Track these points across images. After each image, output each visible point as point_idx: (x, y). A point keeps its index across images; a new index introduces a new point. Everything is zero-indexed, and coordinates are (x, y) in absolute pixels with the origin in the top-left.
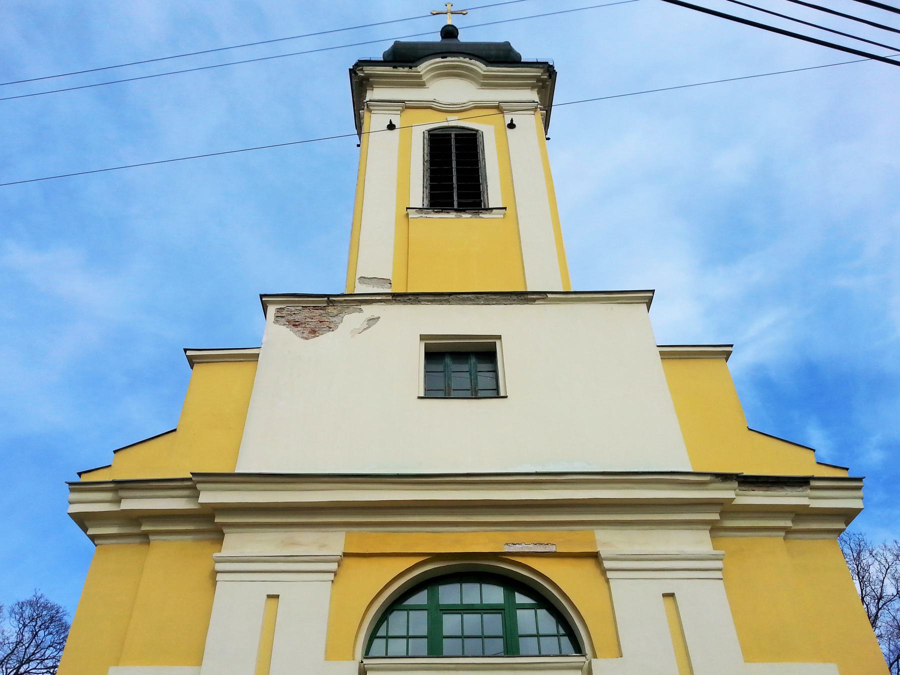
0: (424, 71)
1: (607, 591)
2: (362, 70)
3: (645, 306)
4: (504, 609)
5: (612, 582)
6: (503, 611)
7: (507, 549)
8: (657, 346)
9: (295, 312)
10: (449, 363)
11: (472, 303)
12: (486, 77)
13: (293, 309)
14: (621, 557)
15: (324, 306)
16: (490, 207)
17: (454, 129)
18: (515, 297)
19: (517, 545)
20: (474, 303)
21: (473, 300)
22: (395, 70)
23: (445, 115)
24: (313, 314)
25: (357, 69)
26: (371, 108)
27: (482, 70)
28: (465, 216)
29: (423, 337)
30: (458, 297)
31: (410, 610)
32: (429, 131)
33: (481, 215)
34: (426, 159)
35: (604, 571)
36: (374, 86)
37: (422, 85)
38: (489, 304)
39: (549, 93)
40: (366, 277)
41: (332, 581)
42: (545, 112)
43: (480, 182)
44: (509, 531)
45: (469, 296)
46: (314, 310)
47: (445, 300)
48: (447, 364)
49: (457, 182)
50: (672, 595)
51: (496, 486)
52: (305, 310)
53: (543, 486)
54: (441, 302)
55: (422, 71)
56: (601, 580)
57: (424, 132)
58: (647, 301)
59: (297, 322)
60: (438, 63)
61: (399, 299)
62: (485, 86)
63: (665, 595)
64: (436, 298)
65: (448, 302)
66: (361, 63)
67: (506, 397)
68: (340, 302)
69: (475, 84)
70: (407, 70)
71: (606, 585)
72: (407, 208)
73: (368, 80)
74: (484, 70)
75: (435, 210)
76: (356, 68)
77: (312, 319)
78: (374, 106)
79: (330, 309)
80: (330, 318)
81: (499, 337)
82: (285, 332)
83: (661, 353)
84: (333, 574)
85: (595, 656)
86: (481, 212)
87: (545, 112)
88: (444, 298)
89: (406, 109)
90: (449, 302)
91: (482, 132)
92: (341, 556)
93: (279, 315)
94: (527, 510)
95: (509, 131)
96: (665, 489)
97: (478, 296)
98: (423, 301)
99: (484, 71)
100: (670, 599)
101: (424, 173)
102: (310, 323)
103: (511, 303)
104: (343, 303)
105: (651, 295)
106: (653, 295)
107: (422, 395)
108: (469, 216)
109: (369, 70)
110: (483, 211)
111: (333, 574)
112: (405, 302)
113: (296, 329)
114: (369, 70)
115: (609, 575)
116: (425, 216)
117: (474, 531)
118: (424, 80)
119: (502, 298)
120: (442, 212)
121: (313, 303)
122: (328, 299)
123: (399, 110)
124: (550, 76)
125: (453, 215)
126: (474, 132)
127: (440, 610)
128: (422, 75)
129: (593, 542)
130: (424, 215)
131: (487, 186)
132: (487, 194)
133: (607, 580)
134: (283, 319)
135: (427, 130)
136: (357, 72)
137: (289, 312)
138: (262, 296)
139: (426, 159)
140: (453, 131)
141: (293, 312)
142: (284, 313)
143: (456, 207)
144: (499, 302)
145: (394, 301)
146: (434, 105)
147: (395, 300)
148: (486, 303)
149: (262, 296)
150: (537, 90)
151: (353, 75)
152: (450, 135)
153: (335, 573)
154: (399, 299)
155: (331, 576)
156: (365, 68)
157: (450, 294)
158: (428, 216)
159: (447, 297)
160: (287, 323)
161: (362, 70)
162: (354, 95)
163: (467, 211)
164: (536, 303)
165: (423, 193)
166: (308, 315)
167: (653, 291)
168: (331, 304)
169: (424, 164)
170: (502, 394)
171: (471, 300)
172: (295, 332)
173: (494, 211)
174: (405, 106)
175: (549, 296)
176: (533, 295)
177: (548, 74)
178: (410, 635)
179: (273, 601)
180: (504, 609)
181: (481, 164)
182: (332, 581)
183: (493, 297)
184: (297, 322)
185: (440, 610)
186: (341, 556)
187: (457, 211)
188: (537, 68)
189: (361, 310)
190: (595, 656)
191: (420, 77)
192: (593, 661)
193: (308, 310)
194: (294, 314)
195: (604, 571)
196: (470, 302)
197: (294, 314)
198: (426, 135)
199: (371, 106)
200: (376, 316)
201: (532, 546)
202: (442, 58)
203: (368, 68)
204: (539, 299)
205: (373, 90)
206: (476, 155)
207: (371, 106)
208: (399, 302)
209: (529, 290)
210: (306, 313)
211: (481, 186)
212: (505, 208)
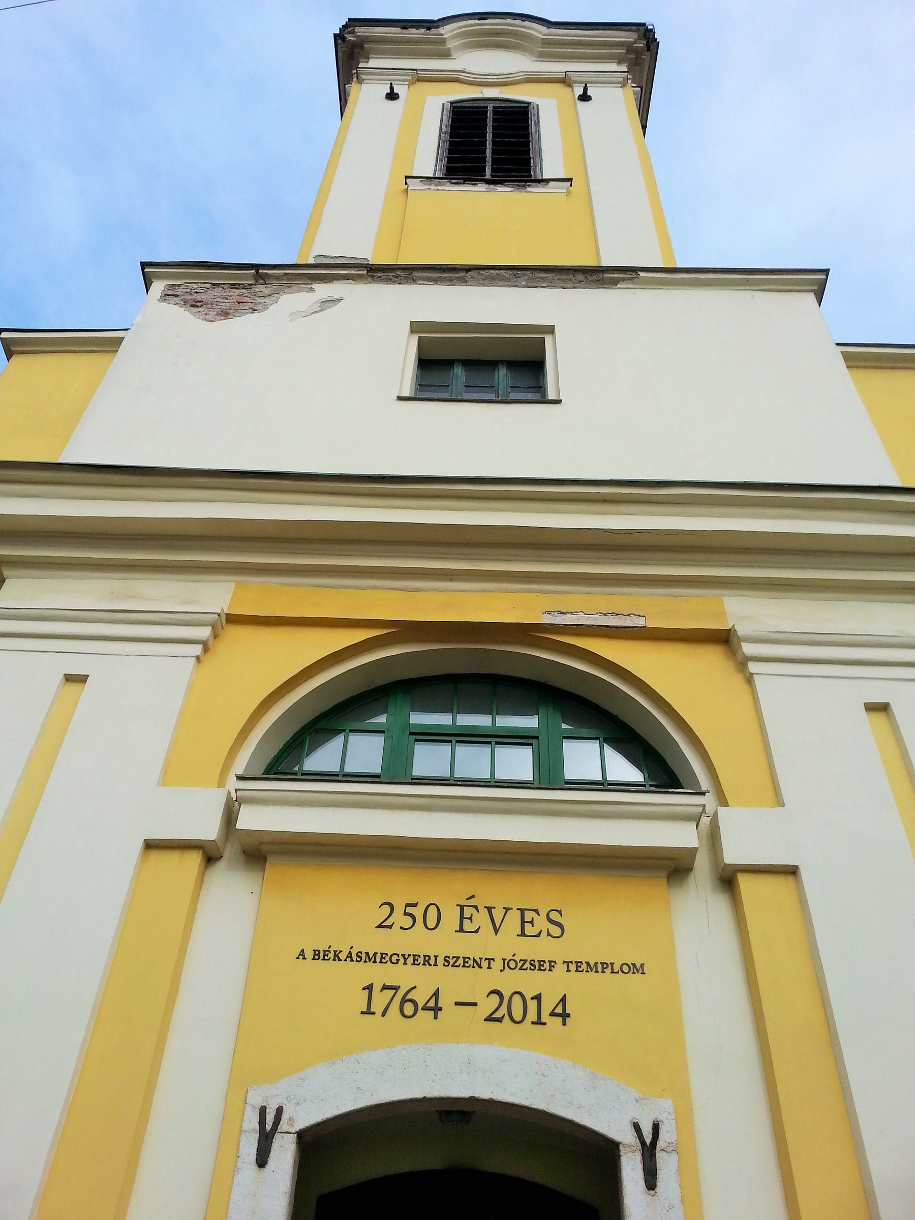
0: (450, 34)
1: (748, 701)
2: (353, 32)
3: (811, 297)
4: (537, 738)
5: (757, 680)
6: (535, 742)
7: (547, 620)
8: (837, 344)
9: (198, 291)
10: (460, 374)
11: (506, 283)
12: (546, 43)
13: (195, 286)
14: (779, 636)
15: (249, 285)
16: (544, 177)
17: (492, 102)
18: (581, 277)
19: (568, 615)
20: (509, 283)
21: (509, 280)
22: (404, 31)
23: (480, 88)
24: (228, 294)
25: (346, 30)
26: (363, 77)
27: (540, 33)
28: (500, 188)
29: (416, 327)
30: (483, 274)
31: (351, 731)
32: (452, 103)
33: (528, 189)
34: (444, 130)
35: (742, 663)
36: (370, 56)
37: (446, 55)
38: (536, 287)
39: (646, 73)
40: (328, 254)
41: (198, 658)
42: (639, 89)
43: (530, 155)
44: (554, 592)
45: (501, 271)
46: (231, 290)
47: (458, 279)
48: (458, 374)
49: (493, 154)
50: (883, 708)
51: (531, 505)
52: (215, 290)
53: (623, 508)
54: (451, 282)
55: (446, 33)
56: (738, 680)
57: (443, 104)
58: (816, 288)
59: (200, 302)
60: (472, 25)
61: (379, 275)
62: (544, 56)
63: (871, 708)
64: (444, 275)
65: (463, 281)
66: (353, 23)
67: (558, 402)
68: (277, 278)
69: (527, 54)
70: (424, 32)
71: (746, 688)
72: (406, 177)
73: (362, 48)
74: (544, 33)
75: (453, 181)
76: (344, 31)
77: (227, 299)
78: (367, 74)
79: (260, 288)
80: (258, 298)
81: (551, 330)
82: (177, 313)
83: (846, 356)
84: (201, 646)
85: (723, 801)
86: (529, 186)
87: (639, 89)
88: (457, 275)
89: (419, 83)
90: (466, 281)
91: (537, 105)
92: (219, 615)
93: (170, 292)
94: (594, 554)
95: (581, 105)
96: (867, 522)
97: (515, 272)
98: (420, 279)
99: (544, 35)
100: (880, 718)
101: (439, 145)
102: (222, 304)
103: (574, 286)
104: (282, 280)
105: (824, 277)
106: (827, 277)
107: (406, 393)
108: (510, 189)
109: (361, 31)
110: (533, 184)
111: (201, 646)
112: (389, 281)
113: (196, 310)
114: (361, 31)
115: (753, 667)
116: (436, 188)
117: (483, 591)
118: (449, 47)
119: (558, 277)
120: (464, 183)
121: (230, 279)
122: (257, 271)
123: (407, 80)
124: (648, 46)
125: (482, 187)
126: (526, 105)
127: (411, 734)
128: (446, 38)
129: (722, 614)
130: (433, 187)
131: (541, 161)
132: (541, 168)
133: (749, 679)
134: (176, 299)
135: (448, 102)
136: (346, 35)
137: (188, 290)
138: (144, 265)
139: (444, 130)
140: (492, 103)
141: (195, 291)
142: (178, 291)
143: (488, 174)
144: (554, 285)
145: (370, 279)
146: (462, 76)
147: (373, 277)
148: (529, 285)
149: (144, 265)
150: (627, 64)
151: (340, 41)
152: (487, 107)
153: (206, 649)
154: (379, 275)
155: (197, 649)
156: (357, 29)
157: (468, 269)
158: (440, 188)
159: (462, 274)
160: (182, 302)
161: (353, 32)
162: (340, 54)
163: (507, 184)
164: (617, 287)
165: (436, 166)
166: (220, 295)
167: (826, 272)
168: (262, 281)
169: (440, 136)
170: (551, 396)
171: (503, 279)
172: (194, 314)
173: (551, 183)
174: (419, 78)
175: (642, 274)
176: (614, 274)
177: (645, 42)
178: (346, 770)
179: (73, 687)
180: (537, 738)
181: (533, 137)
182: (198, 658)
183: (543, 275)
184: (200, 302)
185: (411, 734)
186: (219, 615)
187: (488, 182)
188: (627, 31)
189: (312, 290)
190: (723, 801)
191: (443, 42)
192: (722, 811)
193: (222, 289)
194: (196, 292)
195: (742, 663)
196: (501, 283)
197: (196, 292)
198: (448, 106)
199: (362, 74)
200: (336, 296)
201: (597, 616)
202: (479, 19)
203: (363, 29)
204: (623, 280)
205: (368, 62)
206: (527, 135)
207: (362, 74)
208: (380, 280)
209: (606, 262)
210: (218, 292)
211: (532, 161)
212: (570, 180)
